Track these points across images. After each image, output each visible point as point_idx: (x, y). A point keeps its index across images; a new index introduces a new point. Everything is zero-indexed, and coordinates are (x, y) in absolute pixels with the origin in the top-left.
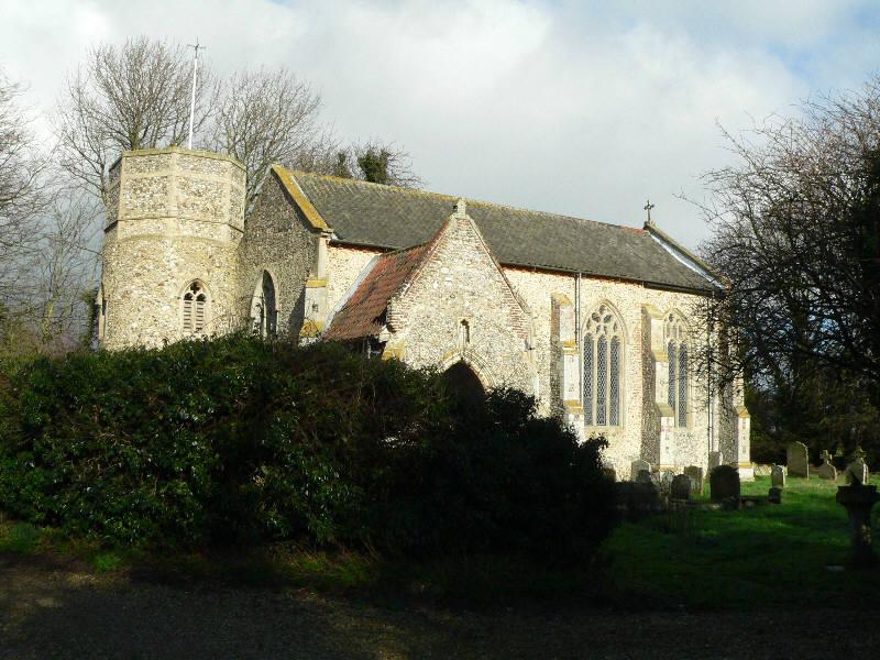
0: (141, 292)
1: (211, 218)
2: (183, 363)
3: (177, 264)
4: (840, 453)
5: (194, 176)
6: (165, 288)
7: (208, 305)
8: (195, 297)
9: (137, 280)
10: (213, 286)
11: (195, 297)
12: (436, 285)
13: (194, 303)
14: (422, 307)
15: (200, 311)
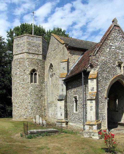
0: (19, 73)
3: (28, 65)
6: (25, 71)
7: (37, 76)
8: (34, 74)
9: (18, 70)
10: (38, 70)
11: (34, 74)
14: (103, 58)
15: (35, 78)
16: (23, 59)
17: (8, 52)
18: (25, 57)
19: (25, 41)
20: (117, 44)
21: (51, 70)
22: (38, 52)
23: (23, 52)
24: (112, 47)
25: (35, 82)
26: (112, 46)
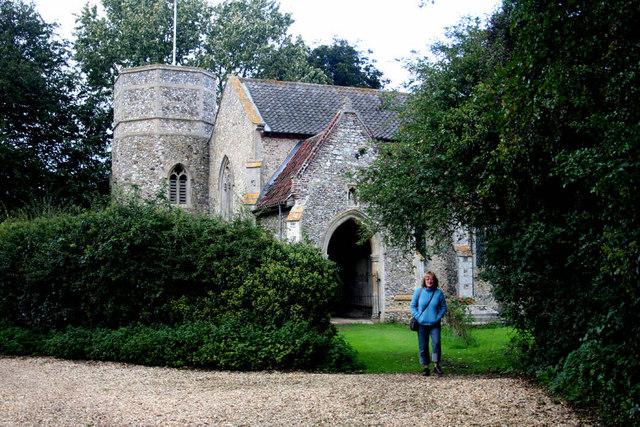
1: (188, 117)
2: (451, 207)
3: (163, 153)
4: (11, 315)
5: (174, 86)
7: (188, 183)
8: (178, 177)
9: (135, 166)
10: (192, 168)
11: (178, 177)
12: (328, 164)
13: (178, 183)
15: (183, 190)
16: (150, 135)
17: (107, 172)
18: (156, 131)
19: (154, 84)
20: (348, 150)
21: (226, 171)
22: (192, 114)
23: (147, 116)
24: (338, 158)
25: (183, 200)
26: (336, 155)
